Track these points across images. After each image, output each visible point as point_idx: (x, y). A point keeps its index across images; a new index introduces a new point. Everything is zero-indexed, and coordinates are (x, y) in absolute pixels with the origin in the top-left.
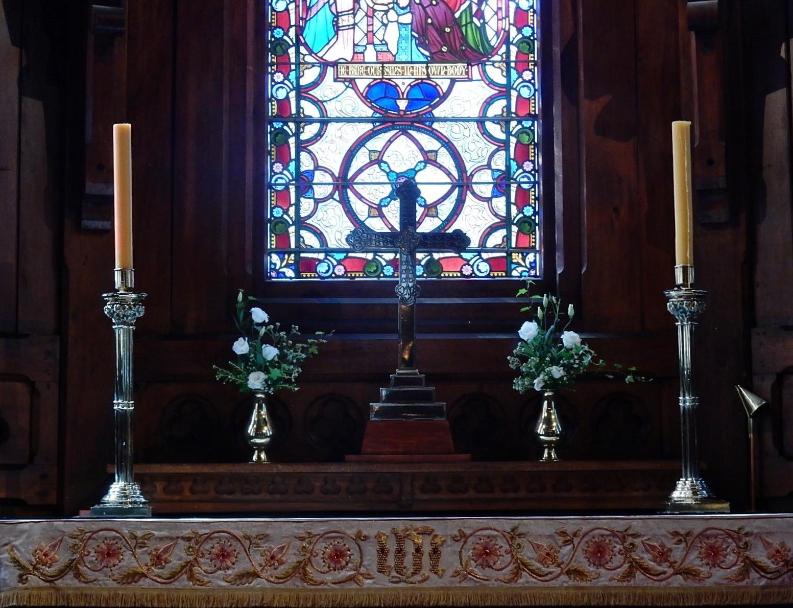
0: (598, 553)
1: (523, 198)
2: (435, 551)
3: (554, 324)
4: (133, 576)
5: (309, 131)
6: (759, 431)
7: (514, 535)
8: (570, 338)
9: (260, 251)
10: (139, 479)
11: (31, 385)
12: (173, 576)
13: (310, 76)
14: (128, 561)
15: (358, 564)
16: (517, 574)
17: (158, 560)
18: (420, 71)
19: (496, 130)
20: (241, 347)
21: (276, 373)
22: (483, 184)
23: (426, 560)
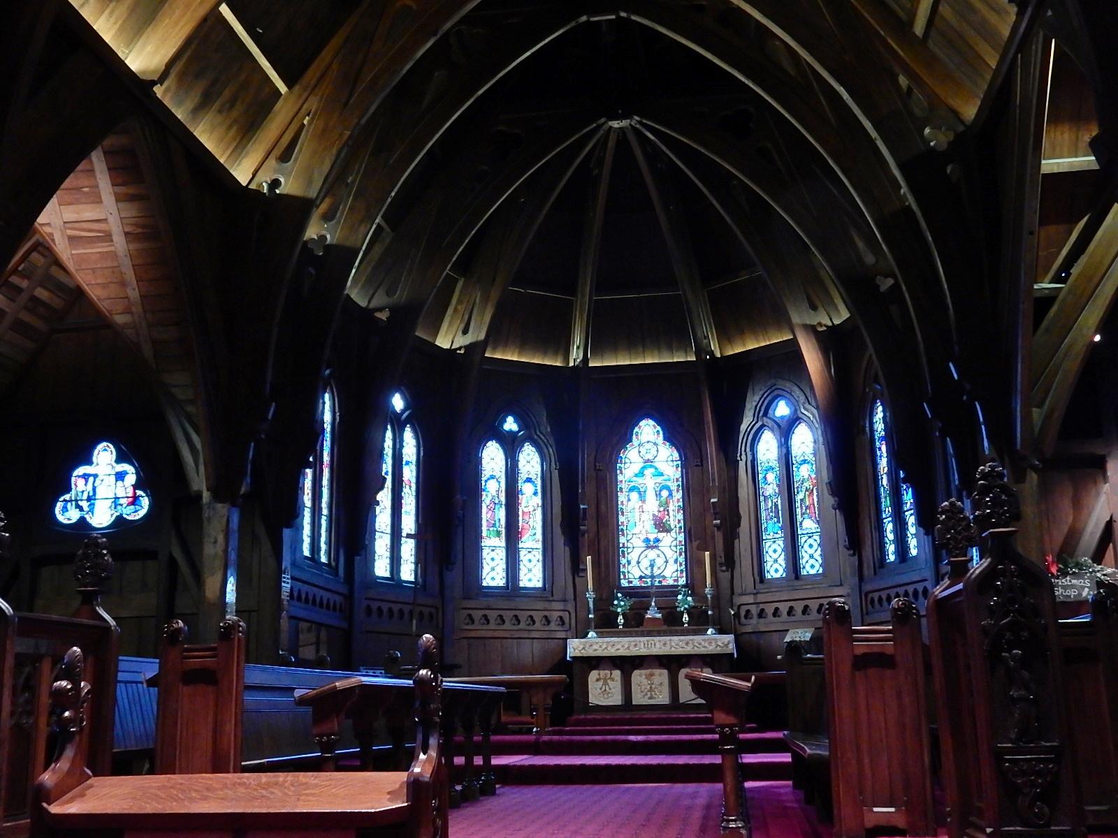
0: (687, 644)
1: (681, 564)
2: (655, 644)
3: (686, 595)
4: (618, 649)
5: (630, 550)
6: (734, 619)
7: (671, 640)
8: (689, 599)
9: (620, 579)
10: (596, 633)
11: (569, 612)
12: (603, 650)
13: (629, 537)
14: (595, 647)
15: (702, 511)
16: (671, 648)
17: (623, 646)
18: (655, 536)
19: (674, 549)
20: (616, 602)
21: (624, 608)
22: (671, 561)
23: (653, 646)
